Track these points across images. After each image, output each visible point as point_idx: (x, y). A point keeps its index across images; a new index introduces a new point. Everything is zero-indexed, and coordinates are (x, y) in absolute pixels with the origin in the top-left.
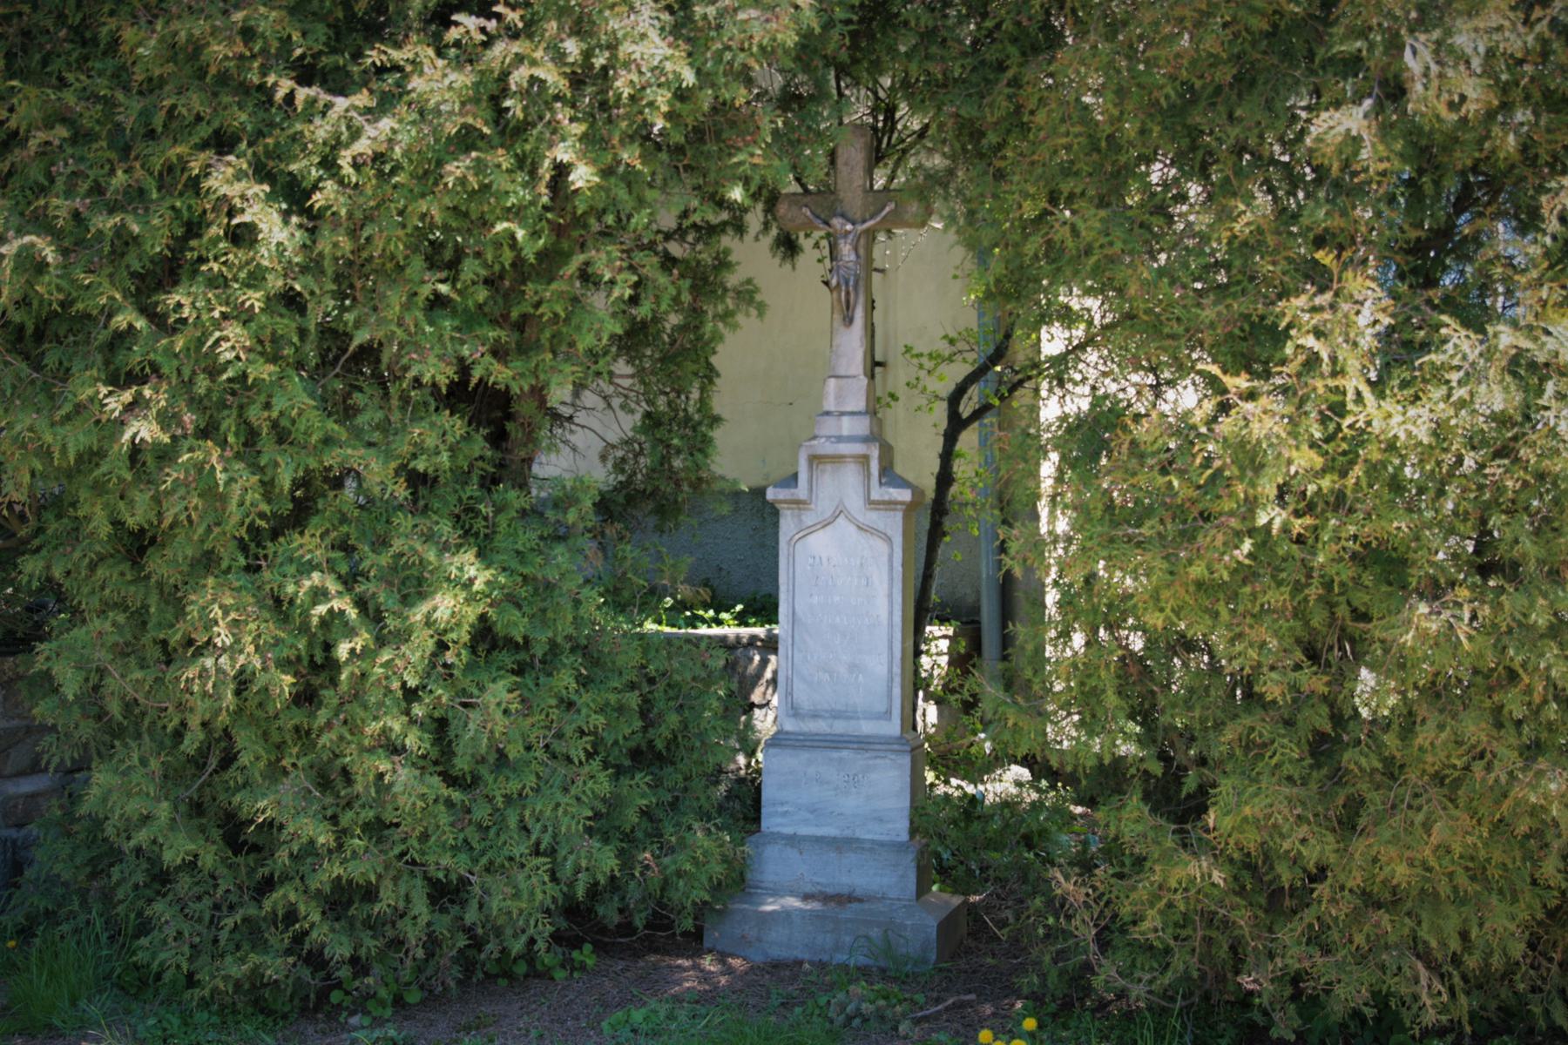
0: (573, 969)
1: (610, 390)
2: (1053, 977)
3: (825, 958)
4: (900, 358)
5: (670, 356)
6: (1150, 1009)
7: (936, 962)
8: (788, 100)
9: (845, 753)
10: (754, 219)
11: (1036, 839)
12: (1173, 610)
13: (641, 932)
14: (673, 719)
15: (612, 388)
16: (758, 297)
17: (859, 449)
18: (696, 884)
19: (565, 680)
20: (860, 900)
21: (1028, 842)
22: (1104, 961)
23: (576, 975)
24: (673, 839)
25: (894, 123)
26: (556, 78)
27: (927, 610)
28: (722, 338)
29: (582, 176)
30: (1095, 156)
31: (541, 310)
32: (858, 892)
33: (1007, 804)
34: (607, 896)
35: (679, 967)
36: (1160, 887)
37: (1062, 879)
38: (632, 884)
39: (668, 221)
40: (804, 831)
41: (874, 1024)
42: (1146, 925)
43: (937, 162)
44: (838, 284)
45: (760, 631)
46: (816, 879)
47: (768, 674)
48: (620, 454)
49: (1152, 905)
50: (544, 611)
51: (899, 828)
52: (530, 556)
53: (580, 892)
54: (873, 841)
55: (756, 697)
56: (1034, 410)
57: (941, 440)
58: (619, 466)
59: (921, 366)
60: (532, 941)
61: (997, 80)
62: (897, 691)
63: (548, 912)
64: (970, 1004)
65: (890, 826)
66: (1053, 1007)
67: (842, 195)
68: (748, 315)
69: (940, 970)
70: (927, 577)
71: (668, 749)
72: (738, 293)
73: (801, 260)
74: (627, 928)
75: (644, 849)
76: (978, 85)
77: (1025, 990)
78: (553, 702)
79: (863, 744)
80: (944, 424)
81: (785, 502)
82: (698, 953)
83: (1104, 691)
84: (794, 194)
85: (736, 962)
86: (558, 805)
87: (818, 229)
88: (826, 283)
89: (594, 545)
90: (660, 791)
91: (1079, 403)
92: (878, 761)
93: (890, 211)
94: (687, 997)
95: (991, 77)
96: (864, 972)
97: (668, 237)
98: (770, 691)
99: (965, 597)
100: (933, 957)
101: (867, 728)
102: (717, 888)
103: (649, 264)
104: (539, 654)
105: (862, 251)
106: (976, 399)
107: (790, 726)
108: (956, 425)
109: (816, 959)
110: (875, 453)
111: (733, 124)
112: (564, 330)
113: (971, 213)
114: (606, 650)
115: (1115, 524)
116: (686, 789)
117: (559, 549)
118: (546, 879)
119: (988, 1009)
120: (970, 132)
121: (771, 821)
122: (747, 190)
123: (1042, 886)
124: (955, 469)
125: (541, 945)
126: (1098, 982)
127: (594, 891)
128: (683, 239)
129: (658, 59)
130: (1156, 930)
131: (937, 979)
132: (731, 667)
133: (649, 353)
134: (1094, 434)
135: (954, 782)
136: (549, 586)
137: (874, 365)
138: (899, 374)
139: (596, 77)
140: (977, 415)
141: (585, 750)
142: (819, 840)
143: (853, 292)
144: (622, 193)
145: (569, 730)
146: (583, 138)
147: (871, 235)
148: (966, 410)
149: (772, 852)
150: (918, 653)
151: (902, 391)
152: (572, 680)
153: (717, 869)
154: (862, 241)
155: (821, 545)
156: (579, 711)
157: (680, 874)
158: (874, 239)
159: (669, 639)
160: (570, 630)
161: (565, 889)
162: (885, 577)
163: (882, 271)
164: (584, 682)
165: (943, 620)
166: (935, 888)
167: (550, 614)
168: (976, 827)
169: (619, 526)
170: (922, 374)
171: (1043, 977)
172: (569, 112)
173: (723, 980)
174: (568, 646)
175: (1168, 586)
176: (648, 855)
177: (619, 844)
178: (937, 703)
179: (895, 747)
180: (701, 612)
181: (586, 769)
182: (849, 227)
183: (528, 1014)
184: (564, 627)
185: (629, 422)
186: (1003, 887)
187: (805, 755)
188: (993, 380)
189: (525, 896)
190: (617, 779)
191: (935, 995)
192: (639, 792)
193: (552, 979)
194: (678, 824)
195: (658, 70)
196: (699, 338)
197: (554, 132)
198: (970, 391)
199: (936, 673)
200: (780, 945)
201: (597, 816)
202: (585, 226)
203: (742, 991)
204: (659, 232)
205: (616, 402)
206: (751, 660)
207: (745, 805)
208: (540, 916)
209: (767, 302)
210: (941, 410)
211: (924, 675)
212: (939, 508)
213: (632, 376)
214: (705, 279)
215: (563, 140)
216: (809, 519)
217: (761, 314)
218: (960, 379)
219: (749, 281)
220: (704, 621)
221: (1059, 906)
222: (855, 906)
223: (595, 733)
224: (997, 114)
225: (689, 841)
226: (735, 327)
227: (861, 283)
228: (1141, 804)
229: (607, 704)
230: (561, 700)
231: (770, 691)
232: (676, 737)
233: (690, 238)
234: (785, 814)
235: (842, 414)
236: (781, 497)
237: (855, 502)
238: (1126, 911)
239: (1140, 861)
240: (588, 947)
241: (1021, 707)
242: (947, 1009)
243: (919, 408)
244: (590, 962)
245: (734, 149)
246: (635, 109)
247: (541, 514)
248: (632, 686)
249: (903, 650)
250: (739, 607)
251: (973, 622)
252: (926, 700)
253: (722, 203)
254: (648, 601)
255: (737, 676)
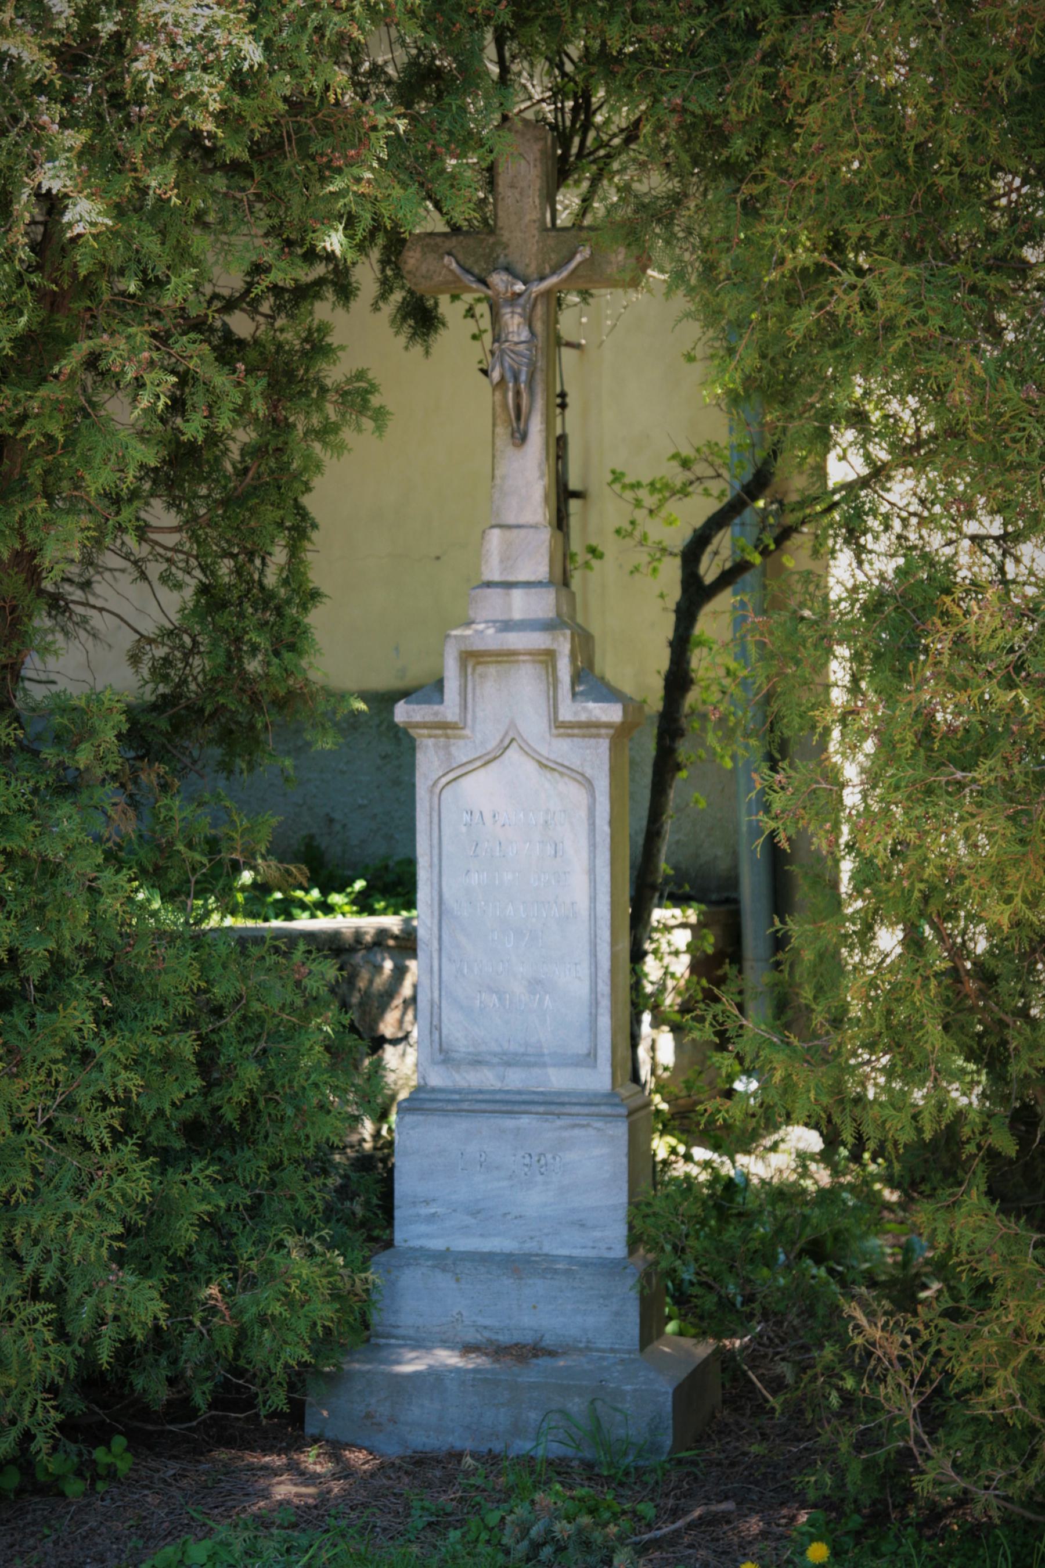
0: (96, 1477)
1: (142, 550)
2: (854, 1476)
3: (498, 1447)
4: (607, 490)
5: (241, 498)
6: (1007, 1522)
7: (674, 1450)
8: (420, 82)
9: (525, 1121)
10: (366, 275)
11: (829, 1244)
12: (1025, 900)
13: (204, 1413)
14: (251, 1073)
15: (146, 548)
16: (375, 401)
17: (538, 640)
18: (290, 1337)
19: (77, 1017)
20: (552, 1353)
21: (816, 1251)
22: (932, 1450)
23: (101, 1486)
24: (253, 1264)
25: (590, 113)
26: (38, 55)
27: (654, 887)
28: (319, 467)
29: (85, 215)
30: (898, 179)
31: (23, 432)
32: (548, 1341)
33: (781, 1194)
34: (149, 1358)
35: (265, 1468)
36: (1017, 1333)
37: (863, 1321)
38: (190, 1339)
39: (231, 280)
40: (464, 1244)
41: (574, 1554)
42: (994, 1394)
43: (655, 183)
44: (503, 378)
45: (392, 922)
46: (482, 1321)
47: (406, 991)
48: (161, 652)
49: (1005, 1361)
50: (41, 907)
51: (612, 1239)
52: (18, 821)
53: (105, 1355)
54: (570, 1259)
55: (388, 1027)
56: (815, 580)
57: (672, 617)
58: (161, 670)
59: (638, 503)
60: (28, 1436)
61: (746, 53)
62: (605, 1022)
63: (53, 1390)
64: (725, 1518)
65: (597, 1234)
66: (855, 1521)
67: (506, 235)
68: (359, 429)
69: (680, 1462)
70: (653, 834)
71: (243, 1120)
72: (344, 394)
73: (443, 340)
74: (181, 1408)
75: (208, 1281)
76: (717, 61)
77: (812, 1495)
78: (58, 1053)
79: (551, 1105)
80: (675, 594)
81: (425, 725)
82: (299, 1443)
83: (921, 1026)
84: (431, 235)
85: (357, 1457)
86: (68, 1217)
87: (469, 290)
88: (485, 372)
89: (121, 799)
90: (231, 1188)
91: (884, 564)
92: (576, 1132)
93: (588, 258)
94: (277, 1517)
95: (738, 46)
96: (559, 1468)
97: (230, 305)
98: (409, 1016)
99: (707, 869)
100: (668, 1442)
101: (559, 1080)
102: (325, 1341)
103: (197, 355)
104: (35, 976)
105: (539, 327)
106: (726, 552)
107: (437, 1079)
108: (694, 595)
109: (484, 1448)
110: (564, 646)
111: (326, 129)
112: (65, 461)
113: (709, 267)
114: (142, 968)
115: (935, 764)
116: (273, 1184)
117: (65, 809)
118: (48, 1336)
119: (754, 1525)
120: (704, 137)
121: (409, 1230)
122: (350, 237)
123: (834, 1325)
124: (694, 664)
125: (41, 1443)
126: (923, 1486)
127: (127, 1352)
128: (253, 308)
129: (203, 22)
130: (1013, 1401)
131: (674, 1477)
132: (341, 993)
133: (203, 491)
134: (907, 616)
135: (700, 1153)
136: (51, 870)
137: (563, 496)
138: (601, 516)
139: (105, 51)
140: (727, 578)
141: (110, 1127)
142: (485, 1258)
143: (532, 388)
144: (151, 244)
145: (84, 1097)
146: (86, 152)
147: (554, 301)
148: (709, 570)
149: (411, 1279)
150: (638, 956)
151: (610, 546)
152: (88, 1017)
153: (325, 1312)
154: (540, 310)
155: (480, 790)
156: (100, 1066)
157: (264, 1321)
158: (559, 302)
159: (245, 941)
160: (85, 938)
161: (80, 1351)
162: (584, 842)
163: (577, 346)
164: (107, 1020)
165: (679, 900)
166: (671, 1327)
167: (51, 914)
168: (732, 1233)
169: (163, 769)
170: (641, 515)
171: (839, 1472)
172: (58, 110)
173: (336, 1487)
174: (82, 963)
175: (1016, 863)
176: (214, 1290)
177: (165, 1275)
178: (672, 1030)
179: (605, 1110)
180: (299, 894)
181: (113, 1157)
182: (519, 287)
183: (22, 1555)
184: (75, 929)
185: (174, 603)
186: (779, 1323)
187: (462, 1125)
188: (759, 514)
189: (15, 1366)
190: (163, 1173)
191: (671, 1502)
192: (198, 1192)
193: (62, 1494)
194: (263, 1241)
195: (204, 41)
196: (284, 467)
197: (37, 143)
198: (715, 541)
199: (670, 983)
200: (425, 1428)
201: (130, 1231)
202: (92, 295)
203: (365, 1505)
204: (215, 296)
205: (154, 570)
206: (379, 968)
207: (366, 1200)
208: (39, 1396)
209: (390, 408)
210: (672, 570)
211: (649, 989)
212: (670, 726)
213: (178, 529)
214: (290, 374)
215: (52, 158)
216: (462, 752)
217: (380, 428)
218: (699, 521)
219: (360, 375)
220: (303, 906)
221: (863, 1362)
222: (543, 1362)
223: (126, 1102)
224: (747, 108)
225: (279, 1269)
226: (340, 449)
227: (539, 377)
228: (985, 1202)
229: (146, 1053)
230: (71, 1050)
231: (409, 1016)
232: (255, 1102)
233: (265, 307)
234: (432, 1218)
235: (509, 585)
236: (417, 718)
237: (533, 724)
238: (965, 1370)
239: (983, 1289)
240: (119, 1442)
241: (794, 1050)
242: (690, 1526)
243: (636, 570)
244: (123, 1466)
245: (326, 171)
246: (168, 106)
247: (36, 753)
248: (186, 1023)
249: (614, 957)
250: (359, 885)
251: (727, 901)
252: (655, 1024)
253: (311, 256)
254: (216, 880)
255: (354, 998)
